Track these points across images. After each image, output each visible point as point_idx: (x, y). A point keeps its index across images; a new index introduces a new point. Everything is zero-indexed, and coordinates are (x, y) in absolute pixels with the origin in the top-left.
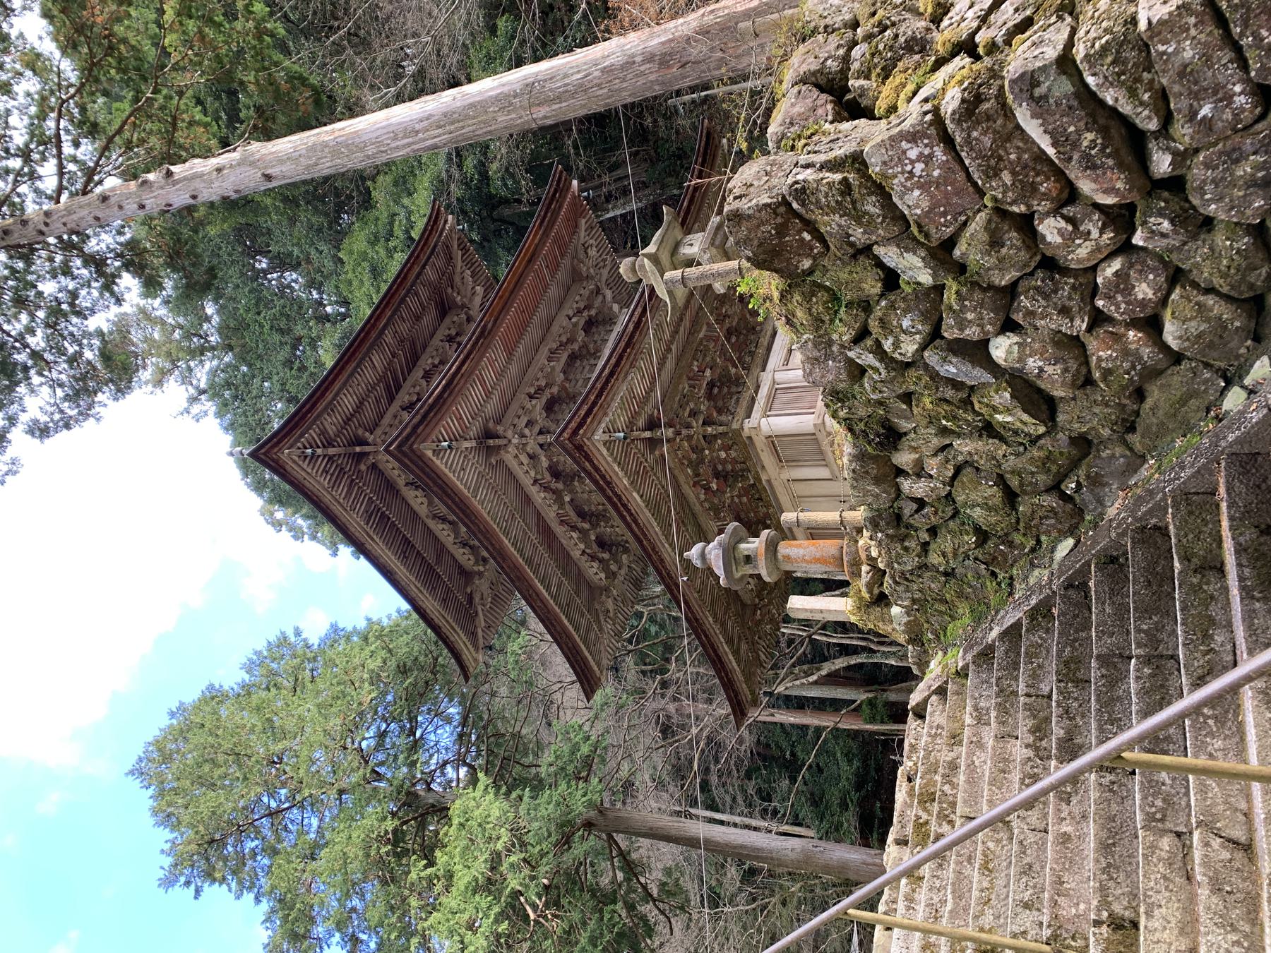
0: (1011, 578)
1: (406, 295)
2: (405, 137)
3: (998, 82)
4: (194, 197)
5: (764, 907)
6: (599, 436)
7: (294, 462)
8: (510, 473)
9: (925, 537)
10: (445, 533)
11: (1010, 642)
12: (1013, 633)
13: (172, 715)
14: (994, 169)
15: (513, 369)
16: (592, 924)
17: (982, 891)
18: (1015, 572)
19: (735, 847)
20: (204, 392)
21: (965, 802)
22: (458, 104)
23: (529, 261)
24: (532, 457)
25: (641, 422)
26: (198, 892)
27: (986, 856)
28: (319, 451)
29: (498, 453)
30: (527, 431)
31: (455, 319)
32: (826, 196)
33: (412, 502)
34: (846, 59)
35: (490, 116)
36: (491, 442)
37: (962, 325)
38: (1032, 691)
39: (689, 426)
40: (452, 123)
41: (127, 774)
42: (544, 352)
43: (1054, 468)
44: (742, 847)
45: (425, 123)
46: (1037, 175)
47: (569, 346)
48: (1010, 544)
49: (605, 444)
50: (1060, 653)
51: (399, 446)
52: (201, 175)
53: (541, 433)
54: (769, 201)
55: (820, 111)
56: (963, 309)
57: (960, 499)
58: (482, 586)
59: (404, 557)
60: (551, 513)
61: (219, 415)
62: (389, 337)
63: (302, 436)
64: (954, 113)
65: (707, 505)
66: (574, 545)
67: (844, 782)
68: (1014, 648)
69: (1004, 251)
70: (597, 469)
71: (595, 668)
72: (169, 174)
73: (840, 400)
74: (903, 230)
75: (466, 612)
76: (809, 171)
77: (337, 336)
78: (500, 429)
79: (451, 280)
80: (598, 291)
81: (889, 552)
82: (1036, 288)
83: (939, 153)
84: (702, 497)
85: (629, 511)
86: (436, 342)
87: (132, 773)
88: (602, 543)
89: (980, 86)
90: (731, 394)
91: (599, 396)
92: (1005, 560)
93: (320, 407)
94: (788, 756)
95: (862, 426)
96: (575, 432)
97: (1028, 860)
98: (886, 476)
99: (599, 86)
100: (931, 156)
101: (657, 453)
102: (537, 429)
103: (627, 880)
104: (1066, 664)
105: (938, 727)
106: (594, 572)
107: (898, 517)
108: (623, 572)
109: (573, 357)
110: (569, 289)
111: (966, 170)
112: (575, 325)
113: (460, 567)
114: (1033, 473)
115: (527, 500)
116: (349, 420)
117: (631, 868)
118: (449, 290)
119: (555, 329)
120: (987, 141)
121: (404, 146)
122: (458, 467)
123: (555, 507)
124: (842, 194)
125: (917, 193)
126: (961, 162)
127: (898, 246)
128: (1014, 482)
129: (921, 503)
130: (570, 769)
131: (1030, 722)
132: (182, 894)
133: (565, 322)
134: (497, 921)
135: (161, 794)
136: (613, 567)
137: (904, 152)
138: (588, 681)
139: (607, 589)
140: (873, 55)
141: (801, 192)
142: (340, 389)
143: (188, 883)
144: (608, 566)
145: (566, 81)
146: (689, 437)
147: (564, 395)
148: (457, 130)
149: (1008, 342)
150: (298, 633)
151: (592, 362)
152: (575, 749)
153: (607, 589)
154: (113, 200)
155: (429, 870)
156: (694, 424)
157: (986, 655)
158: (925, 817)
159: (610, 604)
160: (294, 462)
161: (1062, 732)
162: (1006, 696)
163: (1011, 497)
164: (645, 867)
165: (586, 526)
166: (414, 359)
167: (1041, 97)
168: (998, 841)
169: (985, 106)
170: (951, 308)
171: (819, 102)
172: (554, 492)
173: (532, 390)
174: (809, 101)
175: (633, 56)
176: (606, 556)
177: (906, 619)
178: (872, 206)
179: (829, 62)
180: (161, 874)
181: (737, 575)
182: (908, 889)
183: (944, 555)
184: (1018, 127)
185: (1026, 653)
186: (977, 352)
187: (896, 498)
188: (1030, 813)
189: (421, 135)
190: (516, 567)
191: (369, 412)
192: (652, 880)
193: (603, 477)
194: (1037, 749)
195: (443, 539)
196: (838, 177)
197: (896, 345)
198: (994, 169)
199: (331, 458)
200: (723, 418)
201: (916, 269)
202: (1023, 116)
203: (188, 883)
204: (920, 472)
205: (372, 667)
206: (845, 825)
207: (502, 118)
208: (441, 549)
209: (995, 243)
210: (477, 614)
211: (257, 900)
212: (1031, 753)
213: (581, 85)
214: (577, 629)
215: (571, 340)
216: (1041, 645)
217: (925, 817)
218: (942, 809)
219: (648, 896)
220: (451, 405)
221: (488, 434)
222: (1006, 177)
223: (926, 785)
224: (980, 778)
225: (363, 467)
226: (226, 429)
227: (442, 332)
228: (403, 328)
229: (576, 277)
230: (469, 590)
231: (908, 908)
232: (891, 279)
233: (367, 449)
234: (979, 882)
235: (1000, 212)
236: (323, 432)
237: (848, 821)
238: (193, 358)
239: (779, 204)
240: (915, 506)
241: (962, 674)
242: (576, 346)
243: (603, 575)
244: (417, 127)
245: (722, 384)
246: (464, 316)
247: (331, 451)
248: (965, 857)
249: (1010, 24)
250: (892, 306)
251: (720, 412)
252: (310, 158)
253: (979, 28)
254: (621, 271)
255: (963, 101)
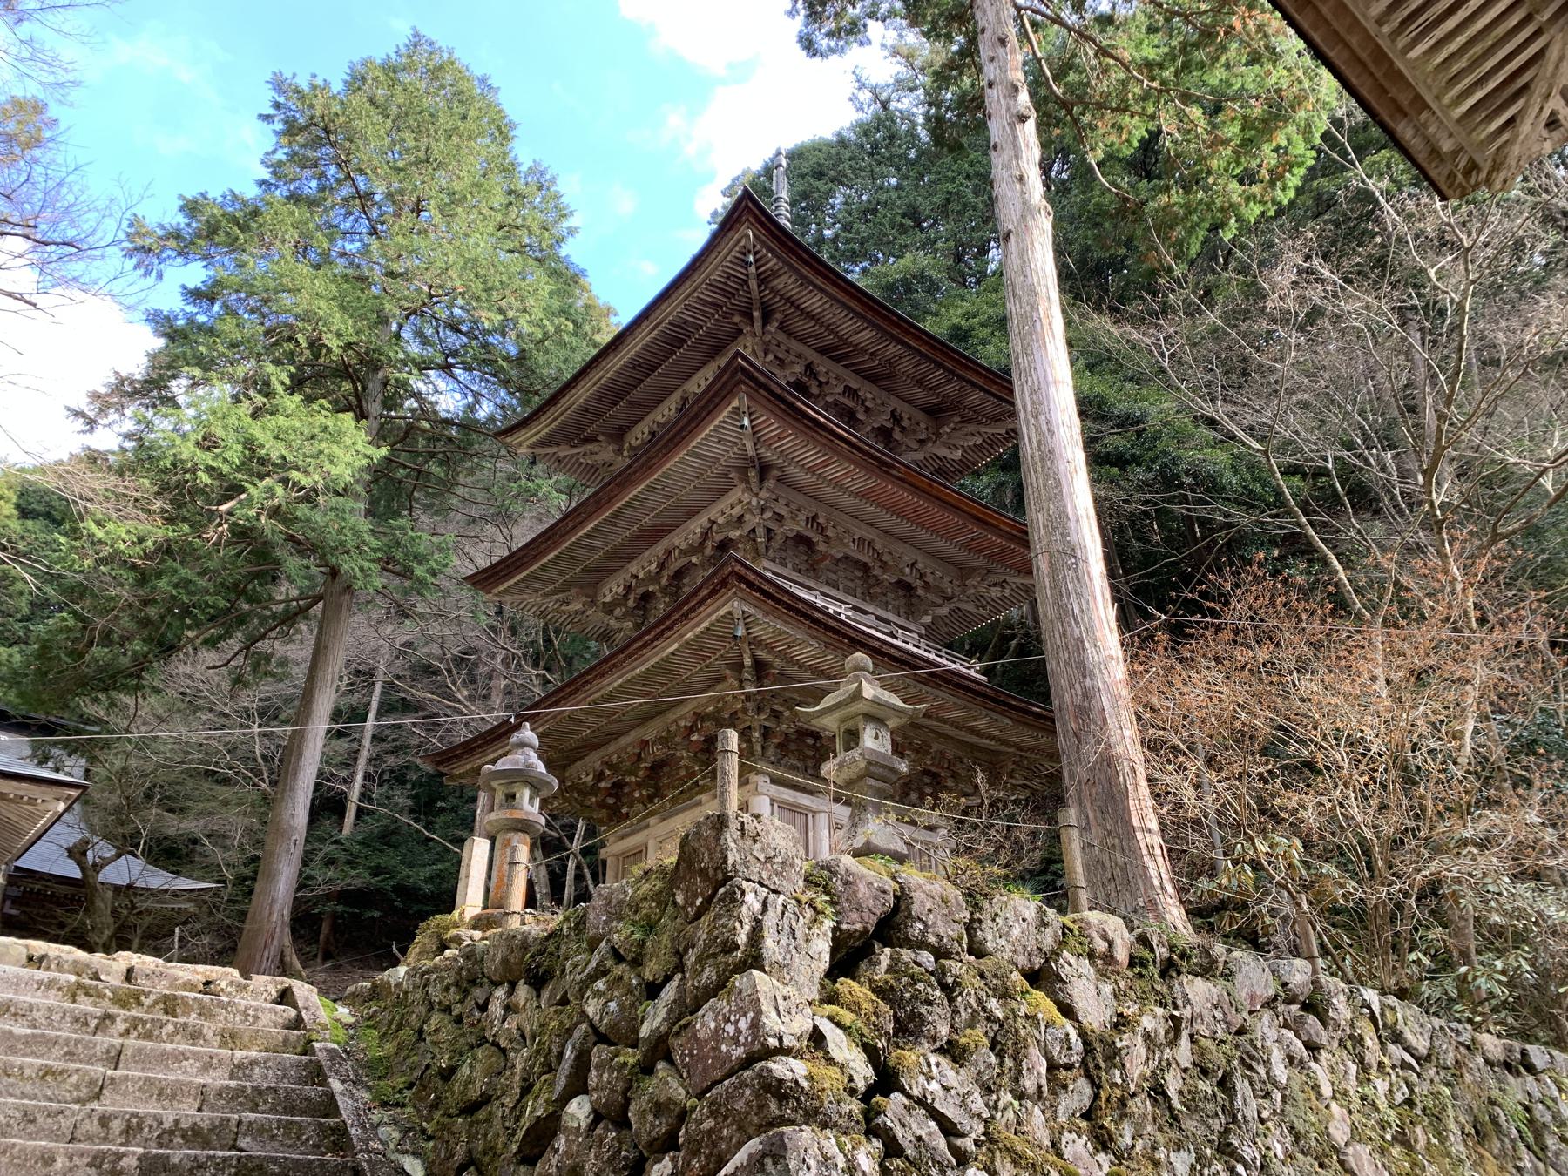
0: (404, 1106)
1: (946, 369)
2: (1033, 403)
3: (799, 1119)
4: (995, 147)
5: (258, 773)
6: (737, 607)
7: (739, 241)
8: (722, 493)
9: (457, 1010)
10: (666, 412)
11: (320, 1104)
12: (329, 1105)
13: (483, 80)
14: (717, 1111)
15: (844, 499)
16: (202, 582)
17: (21, 1068)
18: (408, 1109)
19: (299, 747)
20: (885, 105)
21: (140, 1050)
22: (1062, 467)
23: (978, 519)
24: (740, 518)
25: (761, 654)
26: (267, 118)
27: (61, 1073)
28: (752, 269)
29: (742, 480)
30: (768, 514)
31: (923, 426)
32: (724, 926)
33: (700, 374)
34: (921, 945)
35: (1045, 505)
36: (752, 473)
37: (600, 1067)
38: (244, 1128)
39: (759, 710)
40: (1042, 460)
41: (414, 28)
42: (870, 535)
43: (486, 1159)
44: (300, 755)
45: (1044, 427)
46: (707, 1158)
47: (878, 564)
48: (434, 1106)
49: (730, 613)
50: (275, 1161)
51: (743, 369)
52: (1017, 157)
53: (769, 530)
54: (730, 862)
55: (855, 916)
56: (612, 1069)
57: (480, 1053)
58: (604, 453)
59: (634, 365)
60: (679, 539)
61: (860, 124)
62: (893, 349)
63: (770, 250)
64: (769, 1071)
65: (673, 728)
66: (644, 565)
67: (407, 871)
68: (311, 1108)
69: (650, 1117)
70: (701, 603)
71: (501, 588)
72: (1023, 119)
73: (577, 925)
74: (688, 1007)
75: (575, 434)
76: (757, 906)
77: (933, 273)
78: (770, 483)
79: (970, 421)
80: (948, 599)
81: (448, 969)
82: (619, 1150)
83: (739, 1052)
84: (682, 723)
85: (656, 638)
86: (894, 403)
87: (417, 35)
88: (646, 598)
89: (798, 1099)
90: (804, 759)
91: (788, 607)
92: (421, 1100)
93: (805, 271)
94: (439, 804)
95: (551, 948)
96: (741, 579)
97: (40, 1119)
98: (510, 971)
99: (1064, 634)
100: (737, 1043)
101: (727, 672)
102: (772, 526)
103: (274, 616)
104: (260, 1167)
105: (256, 1018)
106: (613, 588)
107: (473, 982)
108: (612, 622)
109: (865, 568)
110: (951, 563)
111: (721, 1081)
112: (901, 571)
113: (629, 428)
114: (486, 1135)
115: (693, 513)
116: (792, 303)
117: (289, 618)
118: (957, 419)
119: (899, 548)
120: (740, 1105)
121: (1023, 401)
122: (733, 429)
123: (683, 546)
124: (724, 943)
125: (712, 1025)
126: (728, 1076)
127: (674, 1001)
128: (482, 1114)
129: (483, 1008)
130: (398, 555)
131: (205, 1125)
132: (264, 99)
133: (907, 559)
134: (210, 470)
135: (390, 70)
136: (618, 611)
137: (745, 1015)
138: (486, 579)
139: (593, 603)
140: (912, 976)
141: (734, 900)
142: (828, 294)
143: (277, 106)
144: (619, 605)
145: (1073, 596)
146: (745, 711)
147: (817, 557)
148: (1034, 464)
149: (582, 1117)
150: (572, 231)
151: (859, 591)
152: (420, 558)
153: (593, 603)
154: (1000, 50)
155: (280, 389)
156: (763, 717)
157: (317, 1075)
158: (147, 1002)
159: (576, 606)
160: (739, 241)
161: (176, 1161)
162: (254, 1099)
163: (470, 1109)
164: (287, 638)
165: (664, 581)
166: (872, 378)
167: (763, 1165)
168: (77, 1087)
169: (773, 1106)
170: (617, 1056)
171: (866, 915)
172: (701, 544)
173: (821, 520)
174: (871, 903)
175: (1092, 675)
176: (631, 603)
177: (393, 983)
178: (709, 975)
179: (920, 926)
180: (288, 74)
181: (495, 784)
182: (63, 983)
183: (437, 1030)
184: (750, 1138)
185: (291, 1122)
186: (577, 1086)
187: (492, 982)
188: (96, 1122)
189: (1032, 421)
190: (610, 500)
191: (803, 326)
192: (275, 646)
193: (693, 609)
194: (171, 1132)
195: (659, 409)
196: (742, 939)
197: (598, 994)
198: (717, 1111)
199: (746, 282)
200: (771, 751)
201: (654, 1019)
202: (754, 1145)
203: (277, 106)
204: (509, 1009)
205: (522, 321)
206: (353, 873)
207: (1041, 518)
208: (648, 406)
209: (659, 1108)
210: (575, 447)
211: (262, 183)
212: (167, 1126)
213: (1066, 612)
214: (543, 568)
215: (884, 566)
216: (299, 1138)
217: (147, 1002)
218: (144, 1022)
219: (252, 641)
220: (793, 427)
221: (764, 470)
222: (708, 1124)
223: (186, 1004)
224: (167, 1066)
225: (737, 319)
226: (839, 134)
227: (905, 410)
228: (907, 365)
229: (964, 572)
230: (601, 438)
231: (40, 983)
232: (653, 990)
233: (758, 324)
234: (32, 1065)
235: (683, 1115)
236: (775, 274)
237: (358, 876)
238: (927, 94)
239: (725, 872)
240: (481, 1002)
241: (307, 1049)
242: (877, 572)
243: (608, 599)
244: (1042, 417)
245: (817, 749)
246: (923, 436)
247: (753, 284)
248: (73, 1049)
249: (899, 1132)
250: (630, 991)
251: (780, 746)
252: (1022, 288)
253: (909, 1097)
254: (859, 654)
255: (781, 1081)
